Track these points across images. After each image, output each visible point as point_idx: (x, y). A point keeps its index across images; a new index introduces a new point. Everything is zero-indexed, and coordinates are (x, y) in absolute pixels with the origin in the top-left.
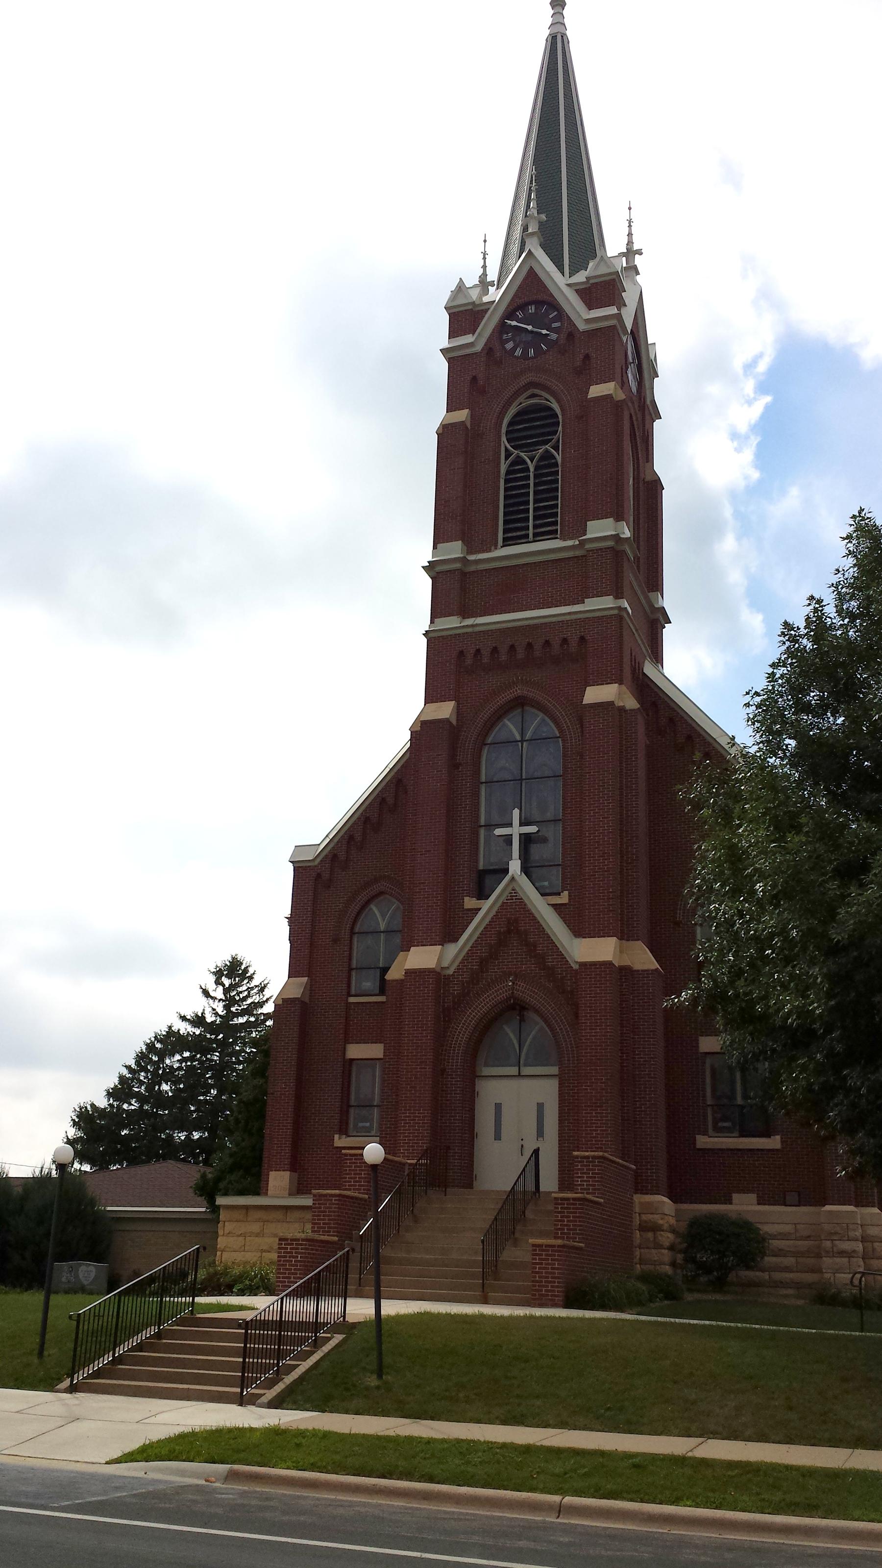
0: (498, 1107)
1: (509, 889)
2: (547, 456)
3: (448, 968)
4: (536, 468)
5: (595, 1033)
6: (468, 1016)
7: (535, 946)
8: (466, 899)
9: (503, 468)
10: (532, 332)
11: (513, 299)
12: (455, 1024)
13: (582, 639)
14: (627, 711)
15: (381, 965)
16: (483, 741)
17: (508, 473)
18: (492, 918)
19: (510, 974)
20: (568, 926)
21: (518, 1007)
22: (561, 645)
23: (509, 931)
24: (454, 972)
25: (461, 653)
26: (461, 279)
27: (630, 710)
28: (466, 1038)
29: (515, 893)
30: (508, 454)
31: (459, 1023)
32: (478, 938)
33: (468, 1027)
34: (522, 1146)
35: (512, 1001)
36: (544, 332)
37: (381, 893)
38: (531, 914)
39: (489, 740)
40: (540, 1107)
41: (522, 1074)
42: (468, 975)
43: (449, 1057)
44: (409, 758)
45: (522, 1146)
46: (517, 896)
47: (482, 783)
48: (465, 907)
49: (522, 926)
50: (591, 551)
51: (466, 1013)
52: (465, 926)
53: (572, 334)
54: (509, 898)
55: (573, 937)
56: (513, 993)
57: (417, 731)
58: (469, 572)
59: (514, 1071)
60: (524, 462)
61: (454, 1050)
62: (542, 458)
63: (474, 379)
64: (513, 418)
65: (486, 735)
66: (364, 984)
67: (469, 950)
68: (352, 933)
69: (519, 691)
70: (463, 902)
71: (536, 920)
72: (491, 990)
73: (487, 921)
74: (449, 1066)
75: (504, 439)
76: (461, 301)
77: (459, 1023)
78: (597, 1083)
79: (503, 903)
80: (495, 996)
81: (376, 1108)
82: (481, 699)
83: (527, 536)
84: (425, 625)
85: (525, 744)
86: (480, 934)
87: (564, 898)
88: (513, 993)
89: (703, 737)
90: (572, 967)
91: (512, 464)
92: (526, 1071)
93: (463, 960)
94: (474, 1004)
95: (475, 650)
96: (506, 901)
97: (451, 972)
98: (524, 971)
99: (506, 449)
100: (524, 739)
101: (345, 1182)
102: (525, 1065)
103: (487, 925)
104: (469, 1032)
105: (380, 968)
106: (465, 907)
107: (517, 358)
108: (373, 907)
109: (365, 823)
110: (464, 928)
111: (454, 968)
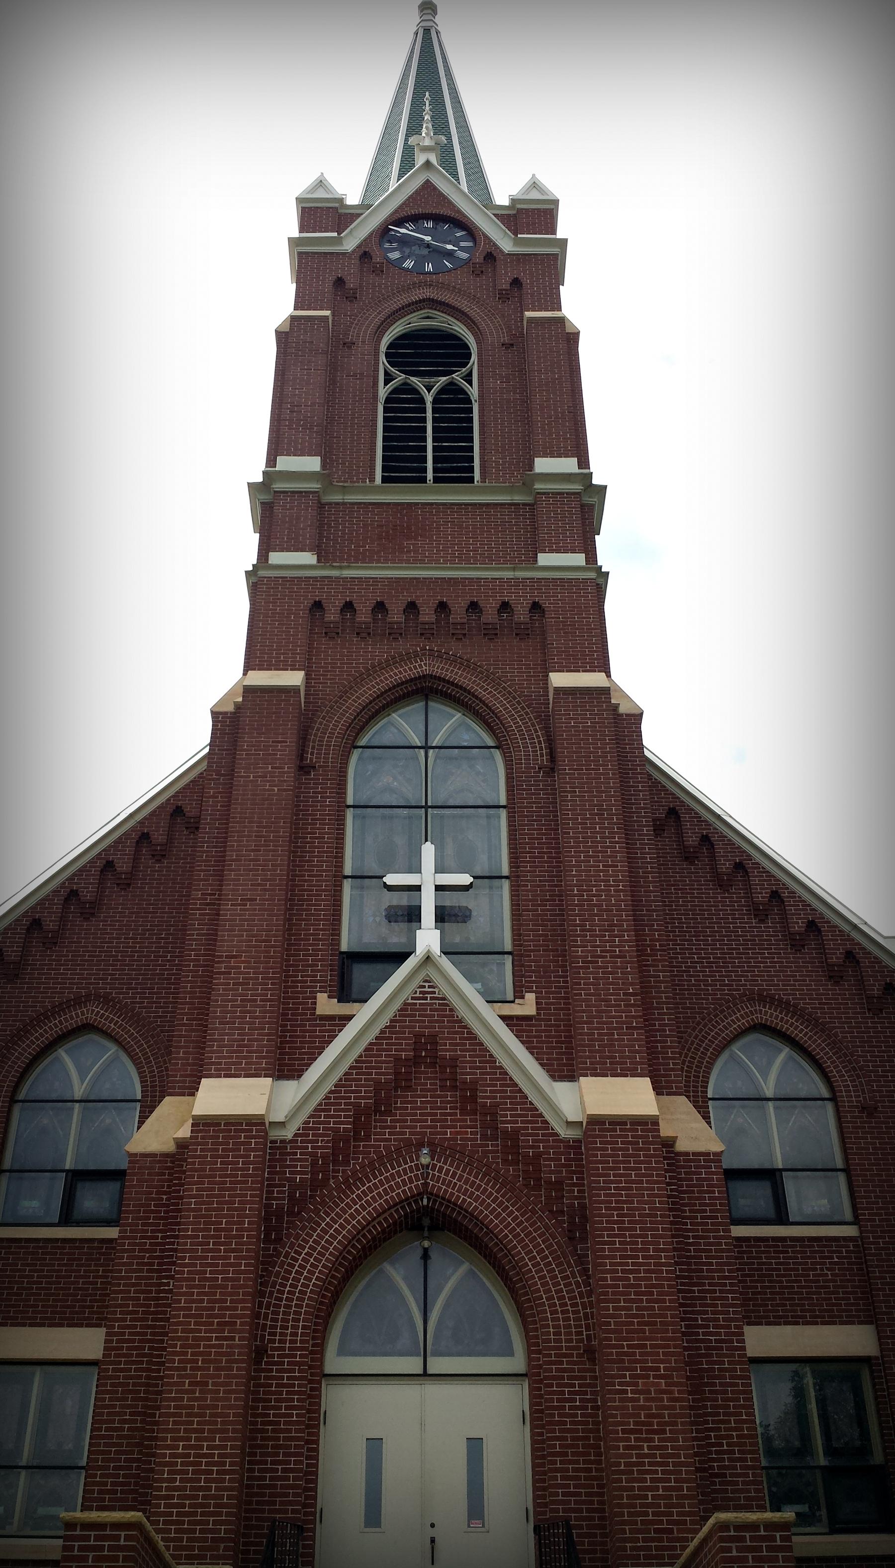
0: (375, 1445)
1: (418, 980)
2: (452, 389)
3: (282, 1124)
4: (435, 401)
5: (633, 1264)
6: (323, 1230)
7: (474, 1091)
8: (322, 998)
9: (383, 392)
10: (428, 246)
11: (401, 207)
12: (291, 1247)
13: (536, 607)
14: (622, 715)
15: (67, 1168)
16: (354, 742)
17: (388, 400)
18: (382, 1032)
19: (420, 1145)
20: (537, 1059)
21: (426, 1222)
22: (499, 612)
23: (416, 1061)
24: (296, 1135)
25: (318, 605)
26: (322, 173)
27: (627, 715)
28: (318, 1279)
29: (429, 987)
30: (388, 378)
31: (300, 1246)
32: (351, 1068)
33: (323, 1255)
34: (433, 1540)
35: (425, 1201)
36: (449, 247)
37: (87, 1028)
38: (465, 1027)
39: (363, 742)
40: (475, 1446)
41: (430, 1371)
42: (328, 1142)
43: (276, 1320)
44: (209, 753)
45: (433, 1540)
46: (435, 993)
47: (349, 807)
48: (319, 1012)
49: (447, 1050)
50: (544, 493)
51: (319, 1225)
52: (317, 1048)
53: (492, 256)
54: (418, 995)
55: (550, 1080)
56: (426, 1184)
57: (226, 713)
58: (330, 504)
59: (413, 1365)
60: (415, 391)
61: (288, 1307)
62: (442, 391)
63: (340, 282)
64: (395, 340)
65: (361, 730)
66: (26, 1203)
67: (331, 1092)
68: (13, 1101)
69: (424, 667)
70: (315, 1003)
71: (475, 1038)
72: (375, 1177)
73: (370, 1037)
74: (274, 1341)
75: (383, 358)
76: (321, 194)
77: (300, 1246)
78: (648, 1377)
79: (405, 1004)
80: (385, 1190)
81: (23, 1473)
82: (344, 679)
83: (424, 480)
84: (250, 558)
85: (431, 752)
86: (356, 1061)
87: (528, 1006)
88: (426, 1184)
89: (696, 813)
90: (557, 1135)
91: (395, 391)
92: (437, 1365)
93: (316, 1110)
94: (337, 1206)
95: (104, 862)
96: (410, 1001)
97: (288, 1133)
98: (449, 1139)
99: (386, 373)
100: (429, 744)
101: (728, 1251)
102: (438, 1354)
103: (371, 1044)
104: (324, 1266)
105: (67, 1171)
106: (319, 1012)
107: (407, 270)
108: (62, 1053)
109: (67, 900)
110: (314, 1053)
111: (296, 1127)
